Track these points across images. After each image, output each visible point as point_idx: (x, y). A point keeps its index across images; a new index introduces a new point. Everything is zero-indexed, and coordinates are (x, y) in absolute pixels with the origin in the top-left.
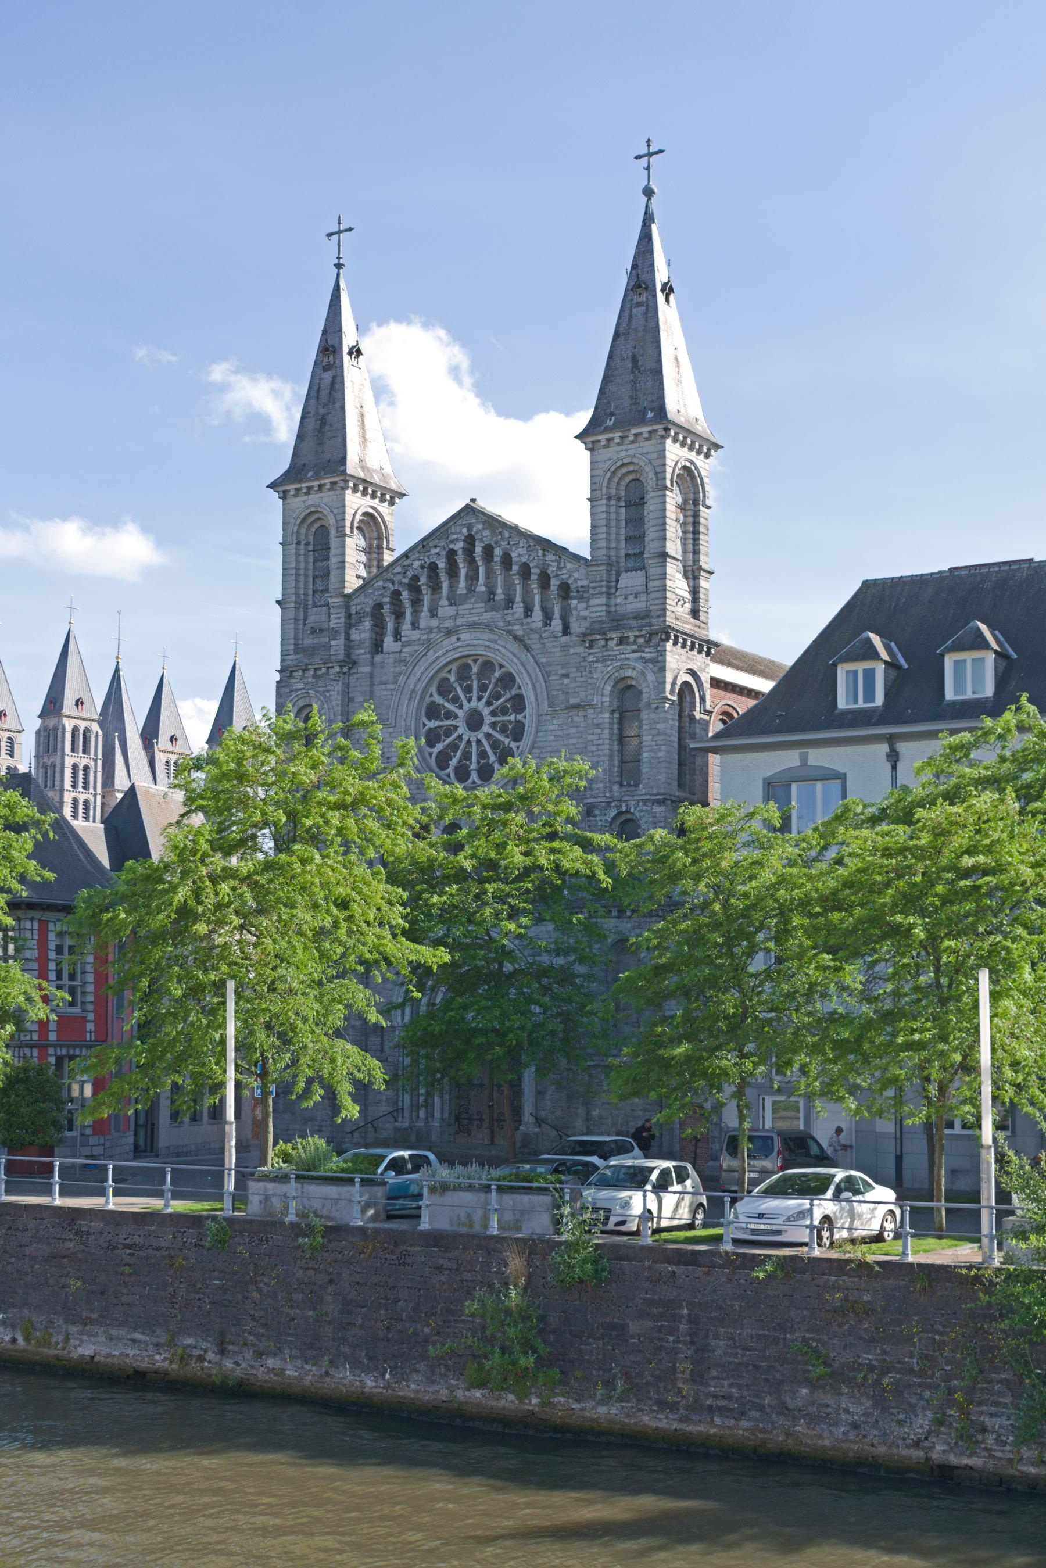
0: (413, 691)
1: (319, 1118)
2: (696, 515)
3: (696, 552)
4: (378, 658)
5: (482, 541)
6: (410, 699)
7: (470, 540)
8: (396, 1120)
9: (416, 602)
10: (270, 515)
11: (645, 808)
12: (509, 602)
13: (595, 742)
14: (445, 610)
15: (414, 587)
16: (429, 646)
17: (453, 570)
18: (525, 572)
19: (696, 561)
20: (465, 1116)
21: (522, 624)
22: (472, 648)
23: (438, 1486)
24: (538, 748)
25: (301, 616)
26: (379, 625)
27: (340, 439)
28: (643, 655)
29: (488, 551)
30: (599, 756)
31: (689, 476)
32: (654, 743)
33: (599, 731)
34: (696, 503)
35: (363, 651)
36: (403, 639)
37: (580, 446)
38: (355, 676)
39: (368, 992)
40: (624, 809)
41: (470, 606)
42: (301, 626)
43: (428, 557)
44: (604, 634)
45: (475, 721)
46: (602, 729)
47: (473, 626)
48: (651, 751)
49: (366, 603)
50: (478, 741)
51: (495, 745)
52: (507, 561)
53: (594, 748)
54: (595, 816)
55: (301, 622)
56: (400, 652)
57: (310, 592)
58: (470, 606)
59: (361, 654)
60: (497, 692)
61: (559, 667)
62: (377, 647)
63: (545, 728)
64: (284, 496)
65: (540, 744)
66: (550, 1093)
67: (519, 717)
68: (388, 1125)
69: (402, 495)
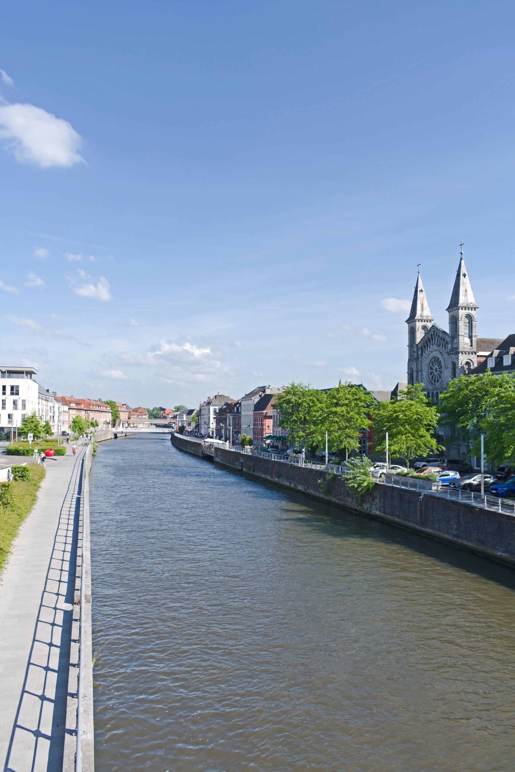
2: (472, 324)
3: (472, 332)
7: (434, 332)
9: (427, 345)
10: (406, 326)
12: (440, 345)
14: (431, 347)
15: (426, 342)
16: (429, 355)
17: (432, 338)
18: (441, 339)
19: (472, 334)
23: (142, 708)
26: (422, 350)
29: (436, 334)
31: (469, 317)
34: (472, 321)
37: (447, 312)
39: (404, 436)
47: (435, 350)
49: (420, 346)
52: (439, 336)
59: (420, 356)
62: (422, 355)
64: (449, 312)
69: (478, 308)
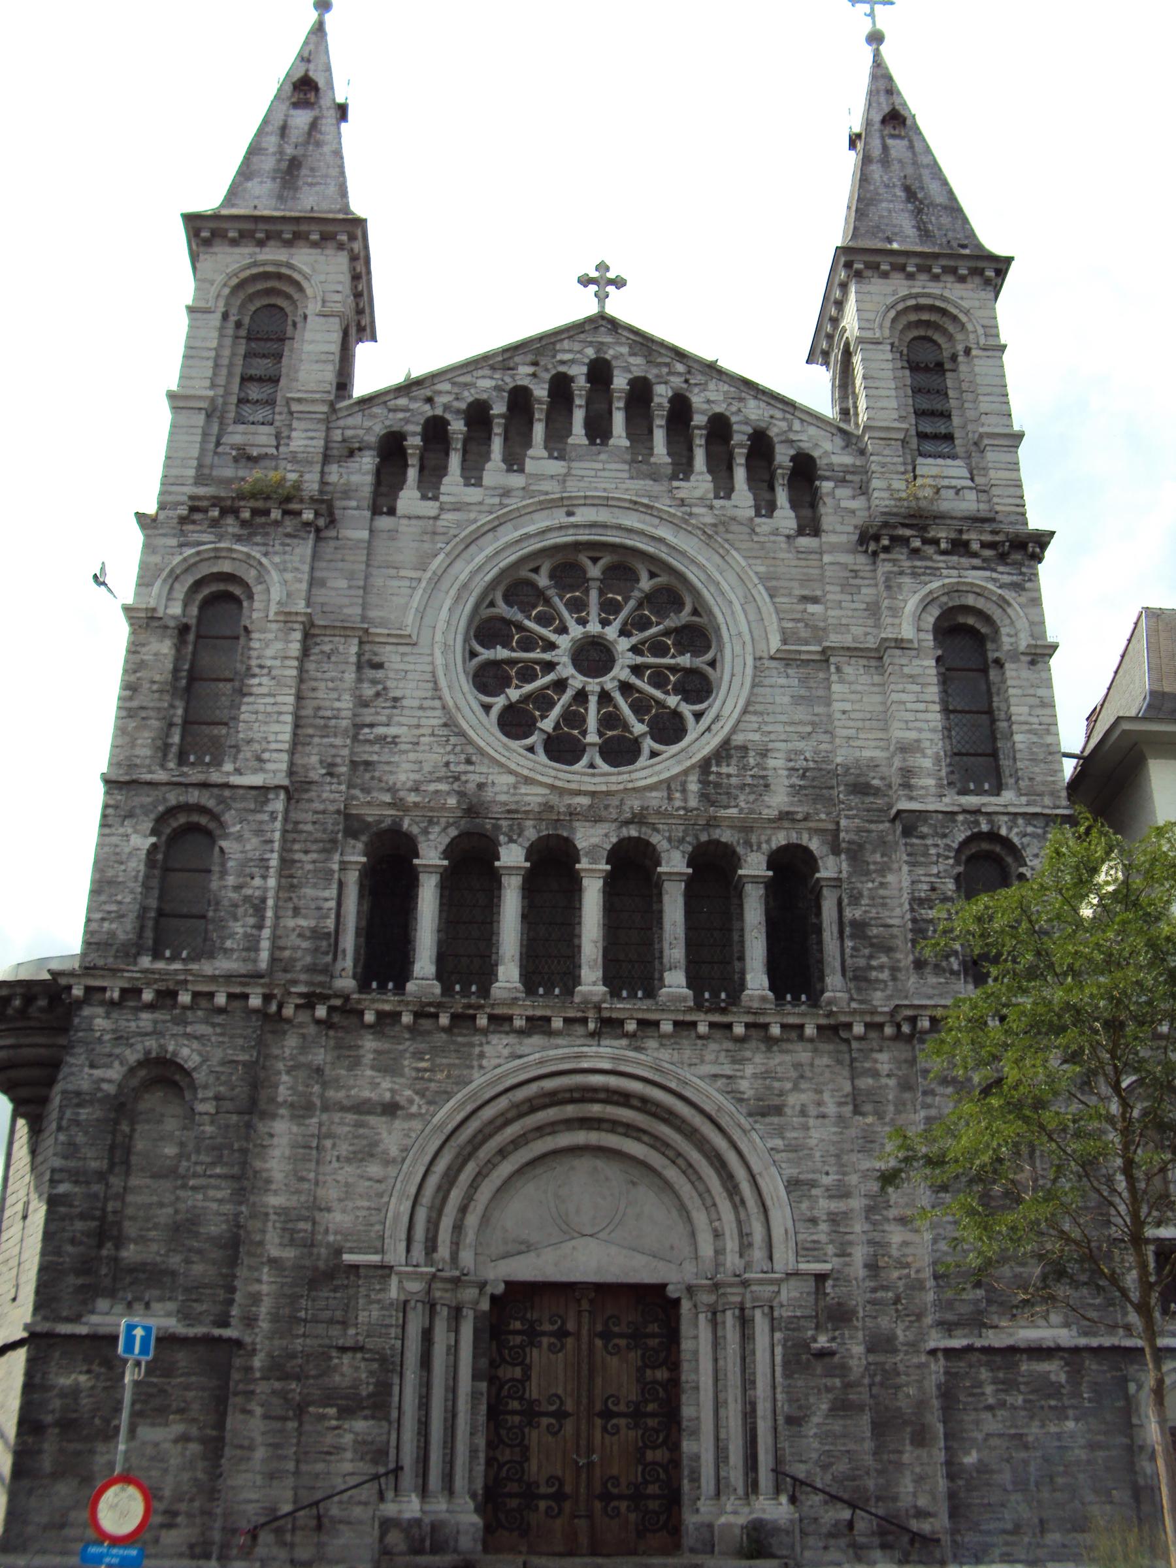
0: (465, 586)
1: (167, 1493)
4: (384, 522)
5: (627, 369)
6: (457, 599)
8: (382, 1497)
11: (1030, 829)
13: (909, 706)
20: (513, 1487)
21: (711, 507)
22: (600, 531)
24: (755, 713)
25: (215, 429)
27: (332, 190)
28: (995, 575)
30: (920, 730)
32: (1034, 720)
33: (917, 688)
35: (354, 504)
36: (443, 498)
38: (332, 544)
40: (985, 827)
41: (600, 466)
42: (212, 446)
43: (513, 376)
44: (924, 528)
45: (591, 655)
46: (923, 685)
48: (1030, 731)
50: (625, 688)
51: (574, 718)
53: (910, 716)
54: (923, 837)
55: (213, 439)
56: (436, 518)
57: (234, 399)
58: (600, 466)
60: (642, 616)
61: (795, 584)
63: (772, 681)
65: (759, 708)
66: (816, 1420)
67: (499, 702)
68: (358, 1512)
